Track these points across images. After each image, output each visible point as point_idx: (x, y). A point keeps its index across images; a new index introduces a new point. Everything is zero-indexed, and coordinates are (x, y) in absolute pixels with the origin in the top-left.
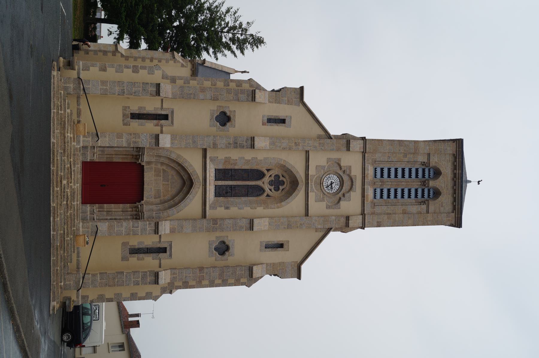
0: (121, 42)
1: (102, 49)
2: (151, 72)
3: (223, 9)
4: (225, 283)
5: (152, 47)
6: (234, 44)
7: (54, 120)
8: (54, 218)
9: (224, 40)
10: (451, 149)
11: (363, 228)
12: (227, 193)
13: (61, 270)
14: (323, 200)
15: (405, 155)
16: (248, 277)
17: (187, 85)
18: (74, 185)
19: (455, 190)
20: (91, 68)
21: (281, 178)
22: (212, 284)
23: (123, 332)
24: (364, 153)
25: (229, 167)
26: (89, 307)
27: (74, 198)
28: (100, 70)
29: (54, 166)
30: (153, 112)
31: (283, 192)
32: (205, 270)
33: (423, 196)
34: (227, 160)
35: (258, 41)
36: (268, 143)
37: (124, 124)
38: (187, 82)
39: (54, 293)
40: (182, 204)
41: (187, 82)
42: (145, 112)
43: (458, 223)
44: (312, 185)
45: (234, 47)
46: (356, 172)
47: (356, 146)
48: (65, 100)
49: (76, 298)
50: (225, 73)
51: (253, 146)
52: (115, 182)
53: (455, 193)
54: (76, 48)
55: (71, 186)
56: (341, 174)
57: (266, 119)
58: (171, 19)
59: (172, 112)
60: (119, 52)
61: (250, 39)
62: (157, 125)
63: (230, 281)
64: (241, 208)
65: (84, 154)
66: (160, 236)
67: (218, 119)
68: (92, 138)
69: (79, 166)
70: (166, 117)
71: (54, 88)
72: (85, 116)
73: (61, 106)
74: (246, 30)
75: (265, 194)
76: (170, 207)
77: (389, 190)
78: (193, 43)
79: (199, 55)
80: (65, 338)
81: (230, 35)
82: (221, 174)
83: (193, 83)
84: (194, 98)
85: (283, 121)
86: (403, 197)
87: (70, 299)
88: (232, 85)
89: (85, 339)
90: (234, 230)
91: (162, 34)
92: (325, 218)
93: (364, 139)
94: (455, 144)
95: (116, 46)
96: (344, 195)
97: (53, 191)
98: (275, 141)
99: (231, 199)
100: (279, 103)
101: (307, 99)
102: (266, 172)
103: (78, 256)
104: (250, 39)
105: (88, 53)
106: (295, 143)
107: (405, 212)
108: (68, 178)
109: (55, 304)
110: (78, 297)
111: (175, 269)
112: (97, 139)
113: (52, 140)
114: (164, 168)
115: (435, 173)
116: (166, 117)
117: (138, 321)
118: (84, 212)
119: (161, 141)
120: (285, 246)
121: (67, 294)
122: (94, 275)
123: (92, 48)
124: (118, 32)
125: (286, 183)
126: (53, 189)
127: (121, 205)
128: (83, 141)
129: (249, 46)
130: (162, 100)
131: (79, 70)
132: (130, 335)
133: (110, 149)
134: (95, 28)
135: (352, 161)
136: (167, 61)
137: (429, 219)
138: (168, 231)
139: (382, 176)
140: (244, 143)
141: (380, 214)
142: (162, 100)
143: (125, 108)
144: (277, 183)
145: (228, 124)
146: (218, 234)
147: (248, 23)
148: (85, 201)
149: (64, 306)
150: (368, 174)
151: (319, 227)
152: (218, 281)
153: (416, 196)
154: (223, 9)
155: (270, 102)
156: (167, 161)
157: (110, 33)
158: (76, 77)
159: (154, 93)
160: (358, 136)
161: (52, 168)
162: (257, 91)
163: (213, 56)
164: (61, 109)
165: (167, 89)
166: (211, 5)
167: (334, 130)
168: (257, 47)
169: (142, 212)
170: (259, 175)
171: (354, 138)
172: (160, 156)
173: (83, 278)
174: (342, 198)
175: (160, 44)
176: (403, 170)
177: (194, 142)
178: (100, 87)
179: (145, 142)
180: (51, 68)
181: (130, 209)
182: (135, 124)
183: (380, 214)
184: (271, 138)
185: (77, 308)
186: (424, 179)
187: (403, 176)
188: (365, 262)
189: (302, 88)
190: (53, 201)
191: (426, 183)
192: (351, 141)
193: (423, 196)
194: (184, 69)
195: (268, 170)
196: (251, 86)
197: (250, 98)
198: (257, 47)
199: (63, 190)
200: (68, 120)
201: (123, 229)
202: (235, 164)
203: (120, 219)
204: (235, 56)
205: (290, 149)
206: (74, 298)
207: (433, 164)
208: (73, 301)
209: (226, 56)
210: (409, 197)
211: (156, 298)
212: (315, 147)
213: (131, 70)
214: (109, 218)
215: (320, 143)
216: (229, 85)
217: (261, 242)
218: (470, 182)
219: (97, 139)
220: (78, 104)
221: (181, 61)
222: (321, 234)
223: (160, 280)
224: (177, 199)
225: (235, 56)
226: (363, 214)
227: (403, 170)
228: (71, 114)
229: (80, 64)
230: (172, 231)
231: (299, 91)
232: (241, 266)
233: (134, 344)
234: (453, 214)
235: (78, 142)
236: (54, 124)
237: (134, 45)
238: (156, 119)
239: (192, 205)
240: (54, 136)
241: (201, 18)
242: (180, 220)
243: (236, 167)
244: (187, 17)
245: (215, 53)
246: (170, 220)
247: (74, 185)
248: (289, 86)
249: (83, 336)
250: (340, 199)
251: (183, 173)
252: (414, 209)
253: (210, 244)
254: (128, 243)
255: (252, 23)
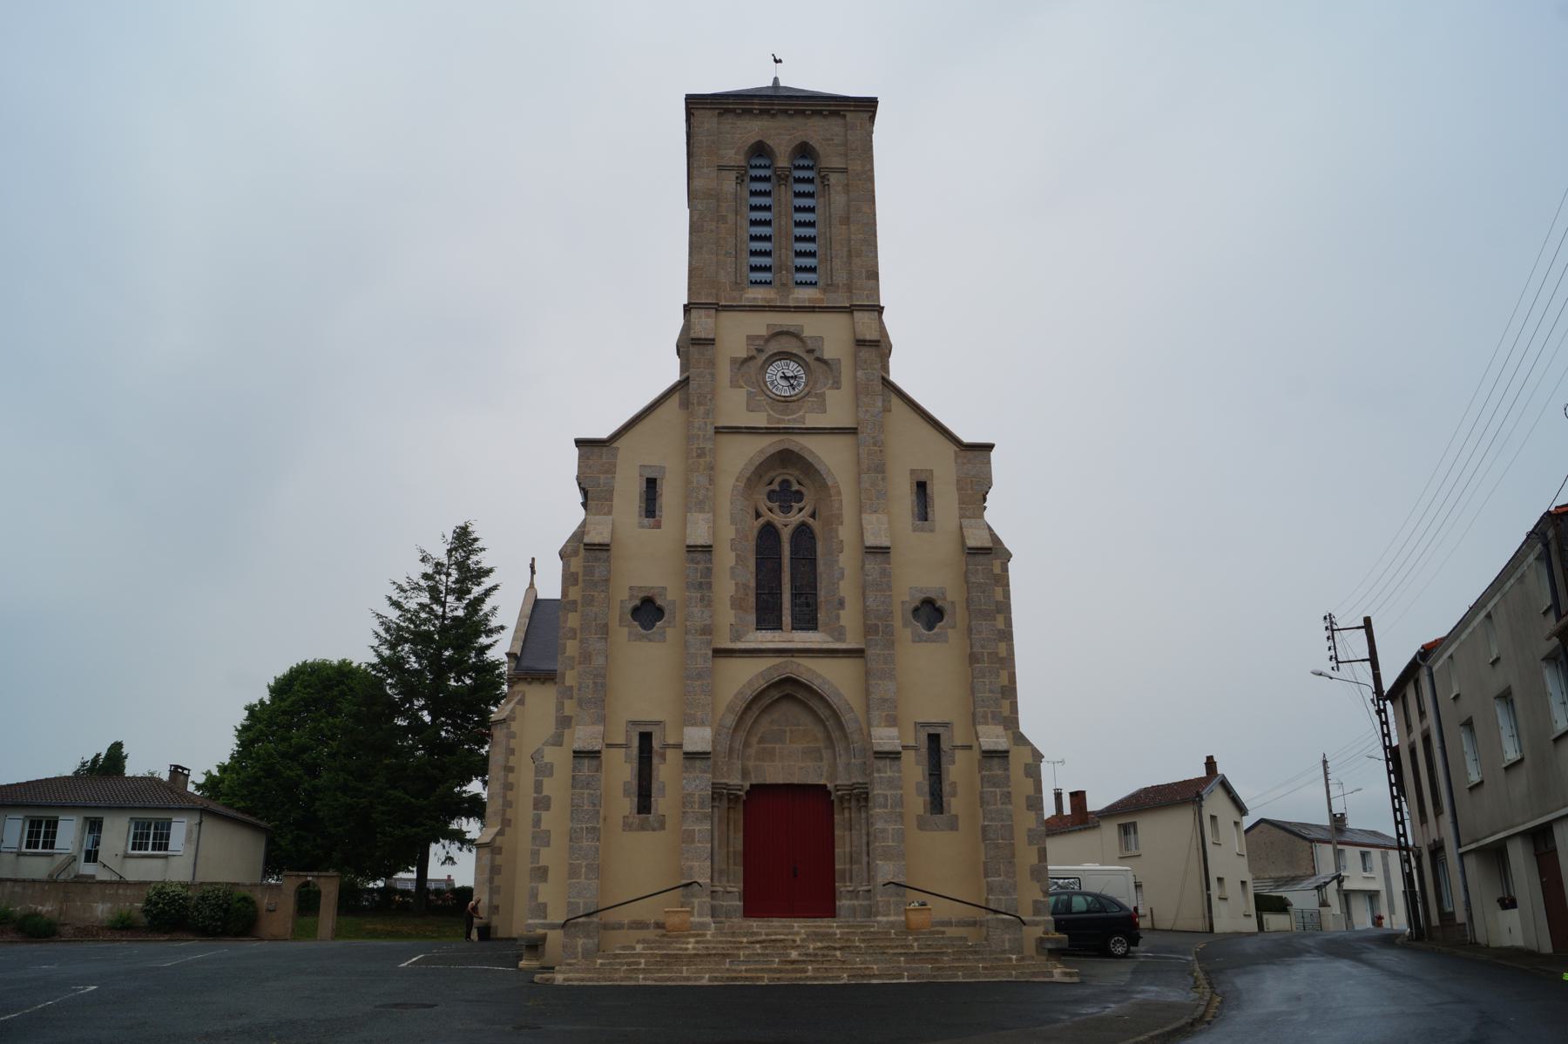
0: (468, 836)
1: (487, 876)
2: (544, 770)
3: (393, 615)
4: (1004, 608)
5: (480, 768)
6: (469, 592)
7: (662, 979)
8: (874, 976)
9: (460, 613)
10: (708, 121)
11: (880, 310)
12: (808, 605)
13: (984, 960)
14: (822, 396)
15: (723, 219)
16: (988, 559)
17: (575, 691)
18: (798, 933)
19: (797, 112)
20: (541, 900)
21: (775, 486)
22: (1006, 635)
23: (1096, 827)
24: (718, 308)
25: (752, 600)
26: (1052, 900)
27: (827, 934)
28: (545, 881)
29: (762, 978)
30: (635, 764)
31: (805, 482)
32: (977, 649)
33: (810, 181)
34: (736, 604)
35: (463, 539)
36: (701, 516)
37: (662, 827)
38: (567, 693)
39: (1034, 974)
40: (833, 700)
41: (567, 693)
42: (635, 783)
43: (868, 106)
44: (788, 421)
45: (476, 591)
46: (759, 324)
47: (705, 324)
48: (617, 956)
49: (1041, 927)
50: (538, 612)
51: (707, 549)
52: (788, 845)
53: (803, 112)
54: (486, 933)
55: (803, 940)
56: (764, 357)
57: (646, 521)
58: (417, 726)
59: (634, 723)
60: (493, 839)
61: (458, 555)
62: (663, 757)
63: (999, 597)
64: (842, 573)
65: (728, 915)
66: (904, 747)
67: (648, 625)
68: (693, 896)
69: (755, 924)
70: (646, 738)
71: (591, 979)
72: (645, 911)
73: (629, 964)
74: (437, 564)
75: (810, 521)
76: (840, 725)
77: (799, 254)
78: (468, 681)
79: (495, 665)
80: (1120, 950)
81: (450, 599)
82: (768, 617)
83: (570, 678)
84: (604, 677)
85: (651, 484)
86: (811, 224)
87: (1041, 941)
88: (575, 594)
89: (1122, 907)
90: (890, 588)
91: (448, 748)
92: (859, 391)
93: (687, 309)
94: (696, 112)
95: (480, 846)
96: (811, 351)
97: (816, 979)
98: (696, 500)
99: (822, 594)
100: (611, 492)
101: (602, 430)
102: (762, 521)
103: (949, 924)
104: (458, 555)
105: (497, 907)
106: (699, 456)
107: (846, 220)
108: (785, 948)
109: (1058, 972)
110: (1037, 924)
111: (974, 714)
112: (696, 887)
113: (705, 982)
114: (754, 740)
115: (760, 156)
116: (646, 738)
117: (1072, 794)
118: (853, 912)
119: (699, 749)
120: (922, 479)
121: (1030, 948)
122: (990, 890)
123: (485, 899)
124: (447, 842)
125: (786, 476)
126: (807, 978)
127: (837, 832)
128: (700, 915)
129: (474, 558)
130: (609, 746)
131: (544, 926)
132: (1101, 811)
133: (716, 858)
134: (438, 892)
135: (736, 334)
136: (511, 736)
137: (859, 168)
138: (894, 731)
139: (767, 269)
140: (700, 567)
141: (850, 273)
142: (609, 746)
143: (627, 826)
144: (786, 496)
145: (659, 602)
146: (897, 623)
147: (422, 560)
148: (750, 911)
149: (1057, 953)
150: (764, 299)
151: (880, 404)
152: (1000, 624)
153: (810, 195)
154: (393, 615)
155: (610, 513)
156: (742, 735)
157: (449, 859)
158: (560, 932)
159: (595, 762)
160: (681, 321)
161: (766, 982)
162: (587, 540)
163: (495, 637)
164: (633, 962)
165: (584, 735)
166: (384, 642)
167: (669, 372)
168: (476, 540)
169: (852, 787)
170: (768, 534)
171: (687, 328)
172: (731, 750)
173: (996, 912)
174: (817, 354)
175: (471, 750)
176: (754, 223)
177: (700, 676)
178: (582, 879)
179: (699, 783)
180: (549, 986)
181: (847, 815)
182: (662, 804)
183: (850, 273)
184: (687, 509)
185: (1059, 926)
186: (774, 179)
187: (767, 223)
188: (955, 307)
189: (579, 443)
190: (838, 978)
191: (781, 178)
192: (693, 335)
193: (810, 181)
194: (529, 699)
195: (758, 515)
196: (575, 553)
197: (603, 555)
198: (476, 540)
199: (812, 958)
200: (659, 948)
201: (890, 827)
202: (746, 586)
203: (868, 834)
204: (495, 588)
205: (712, 468)
206: (1038, 932)
207: (740, 160)
208: (1046, 933)
209: (495, 609)
210: (811, 210)
211: (1038, 756)
212: (707, 413)
213: (544, 815)
214: (865, 859)
215: (699, 404)
216: (575, 602)
217: (914, 530)
218: (776, 79)
219: (696, 887)
220: (620, 926)
221: (511, 706)
222: (895, 400)
223: (1000, 748)
224: (823, 712)
225: (495, 588)
226: (850, 310)
227: (754, 223)
228: (644, 941)
229: (521, 923)
230: (892, 721)
231: (585, 449)
232: (966, 572)
233: (1121, 801)
234: (849, 115)
235: (704, 926)
236: (669, 979)
237: (475, 808)
238: (650, 759)
239: (836, 678)
240: (696, 979)
241: (413, 664)
242: (868, 706)
243: (753, 584)
244: (409, 692)
245: (489, 632)
246: (869, 725)
247: (798, 933)
248: (574, 471)
249: (1114, 912)
250: (818, 359)
251: (766, 701)
252: (838, 199)
253: (918, 639)
254: (919, 816)
255: (422, 551)
